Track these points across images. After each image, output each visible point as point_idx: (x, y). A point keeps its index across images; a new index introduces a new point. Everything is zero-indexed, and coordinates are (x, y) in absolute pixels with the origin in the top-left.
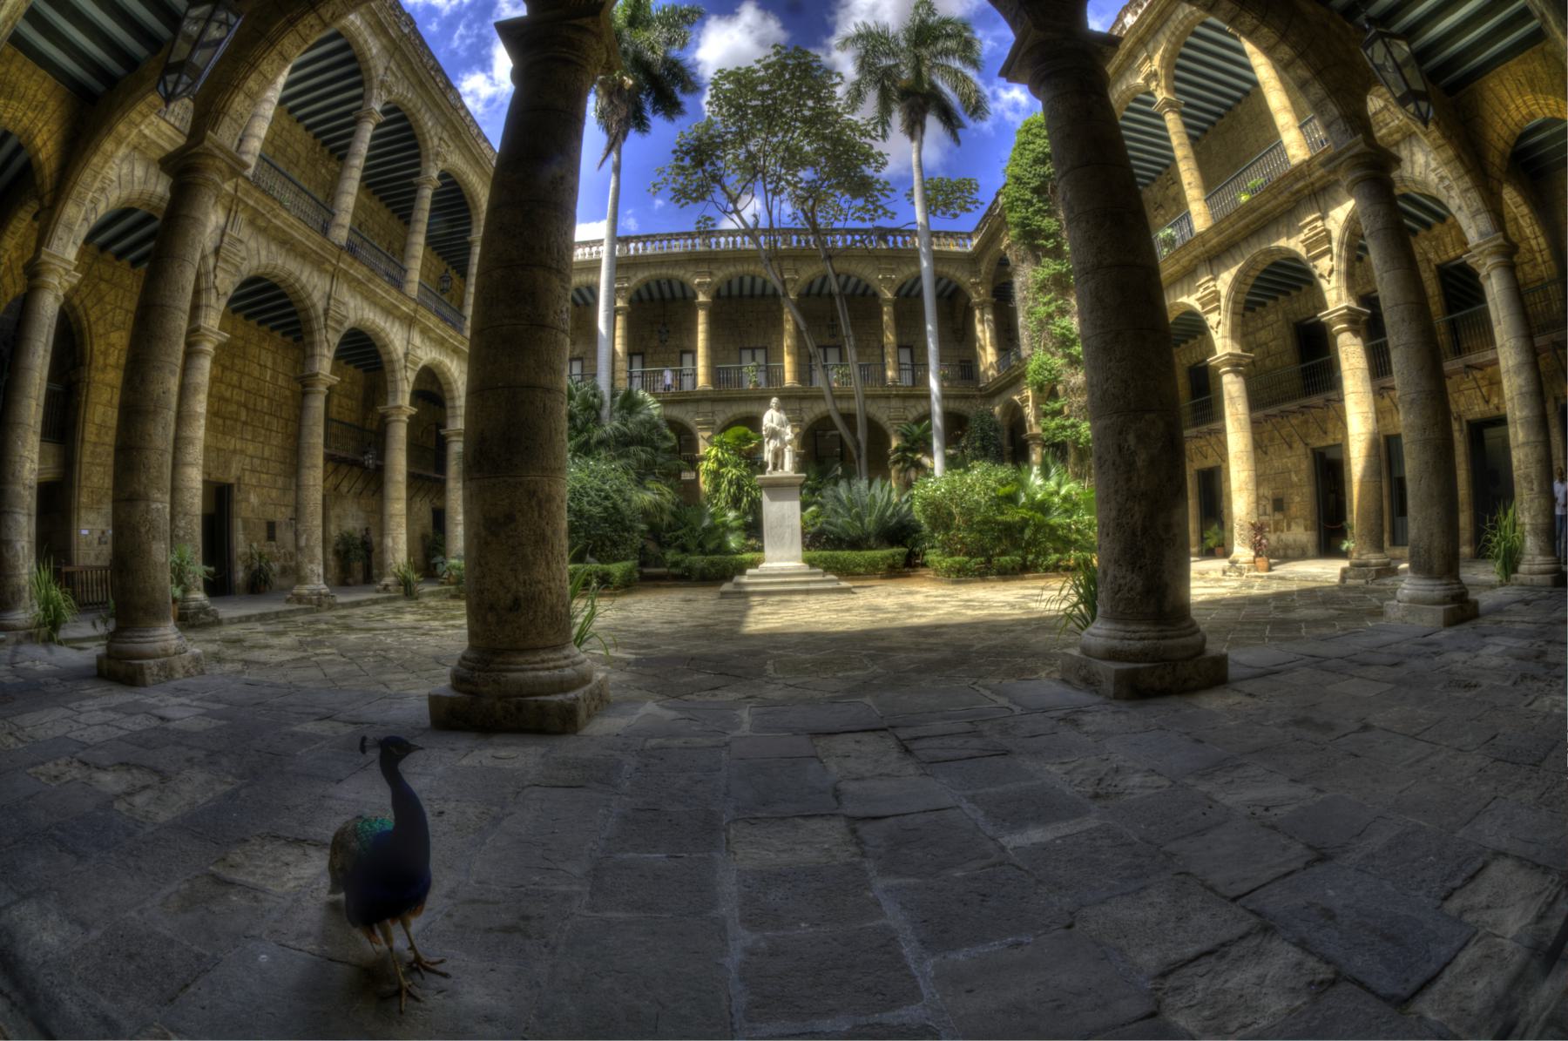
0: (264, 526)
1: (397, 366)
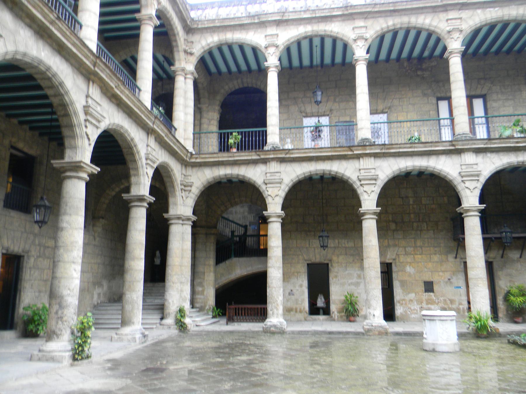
0: (423, 285)
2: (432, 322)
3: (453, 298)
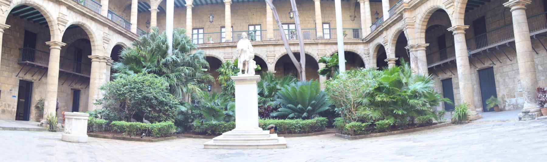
1: (53, 24)
2: (78, 121)
3: (10, 103)
